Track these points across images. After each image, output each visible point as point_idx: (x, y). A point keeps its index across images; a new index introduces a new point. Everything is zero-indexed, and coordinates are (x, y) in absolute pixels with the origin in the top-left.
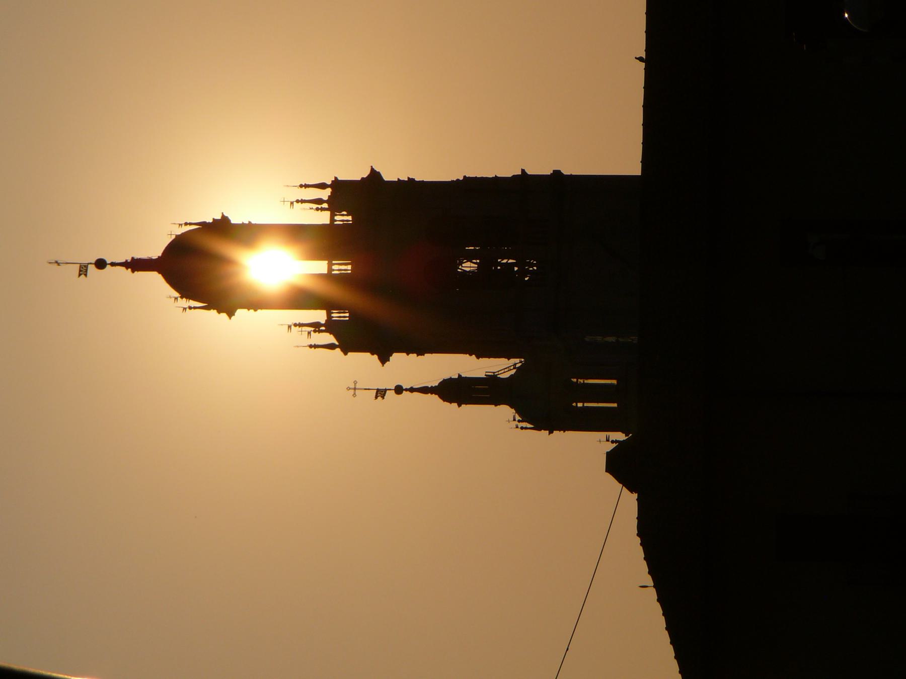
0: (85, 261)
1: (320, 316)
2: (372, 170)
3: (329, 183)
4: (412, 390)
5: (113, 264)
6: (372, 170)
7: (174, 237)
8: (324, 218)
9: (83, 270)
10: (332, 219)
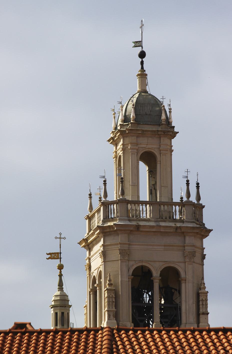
0: (106, 177)
1: (113, 196)
2: (211, 230)
3: (201, 202)
4: (61, 276)
5: (142, 63)
6: (211, 230)
7: (161, 100)
8: (176, 199)
9: (138, 44)
10: (176, 204)
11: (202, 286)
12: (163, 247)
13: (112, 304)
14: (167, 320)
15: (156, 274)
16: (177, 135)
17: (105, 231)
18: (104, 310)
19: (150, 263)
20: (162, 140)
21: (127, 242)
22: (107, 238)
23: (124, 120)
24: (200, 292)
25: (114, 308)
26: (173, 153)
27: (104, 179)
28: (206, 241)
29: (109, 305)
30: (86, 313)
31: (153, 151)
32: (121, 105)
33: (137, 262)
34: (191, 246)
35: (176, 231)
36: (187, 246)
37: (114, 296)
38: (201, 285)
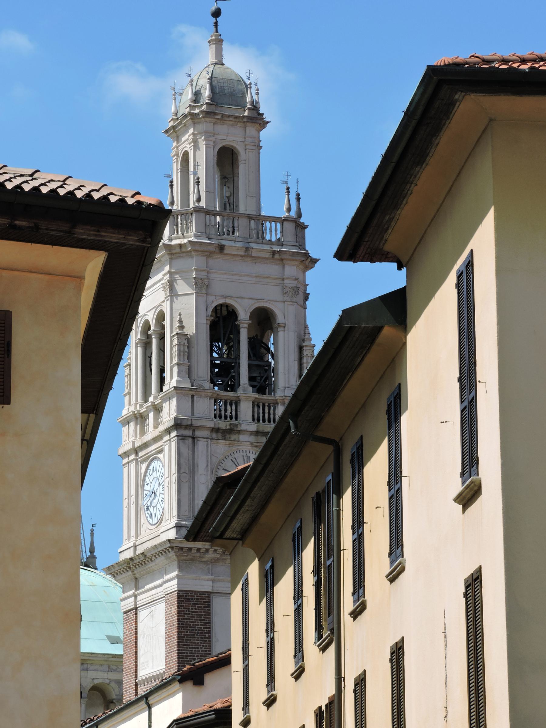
5: (216, 25)
11: (307, 337)
12: (254, 279)
13: (184, 355)
14: (255, 383)
17: (173, 252)
18: (171, 363)
19: (236, 299)
21: (205, 269)
22: (174, 262)
23: (195, 100)
24: (304, 344)
25: (186, 360)
26: (261, 151)
27: (170, 179)
28: (310, 275)
29: (179, 356)
30: (130, 375)
32: (189, 79)
33: (218, 298)
35: (273, 257)
36: (288, 279)
37: (186, 344)
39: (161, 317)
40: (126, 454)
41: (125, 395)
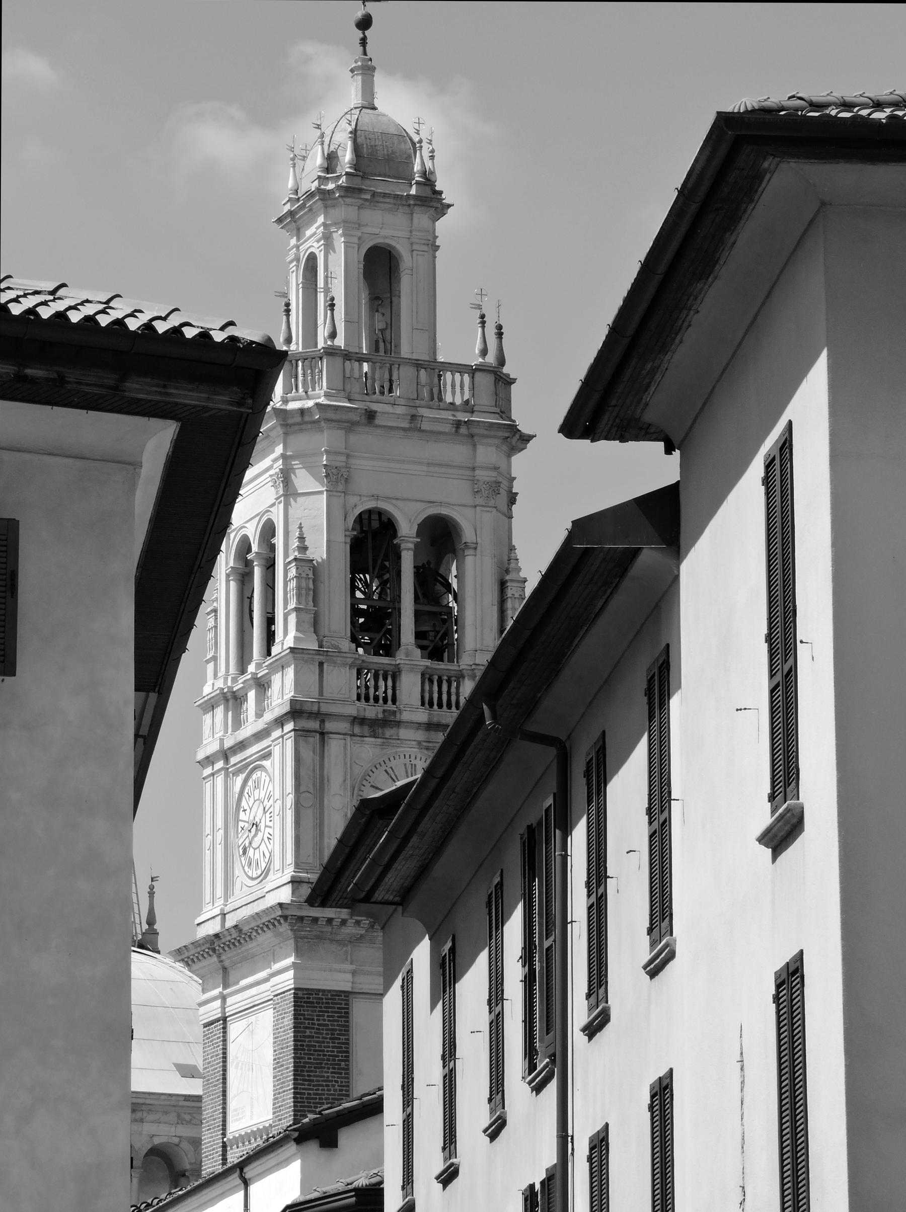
5: (364, 42)
11: (512, 565)
12: (425, 468)
13: (307, 594)
15: (407, 530)
16: (450, 210)
17: (290, 421)
18: (285, 607)
19: (394, 501)
20: (415, 220)
23: (327, 169)
24: (508, 578)
25: (311, 603)
30: (216, 627)
31: (393, 243)
32: (318, 132)
33: (364, 499)
34: (488, 468)
35: (457, 431)
36: (481, 468)
37: (311, 576)
38: (509, 564)
39: (268, 531)
40: (209, 760)
41: (208, 662)
